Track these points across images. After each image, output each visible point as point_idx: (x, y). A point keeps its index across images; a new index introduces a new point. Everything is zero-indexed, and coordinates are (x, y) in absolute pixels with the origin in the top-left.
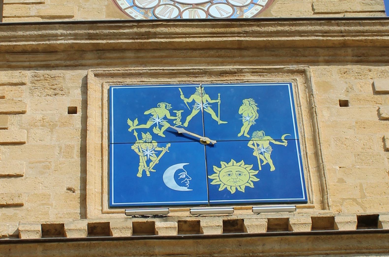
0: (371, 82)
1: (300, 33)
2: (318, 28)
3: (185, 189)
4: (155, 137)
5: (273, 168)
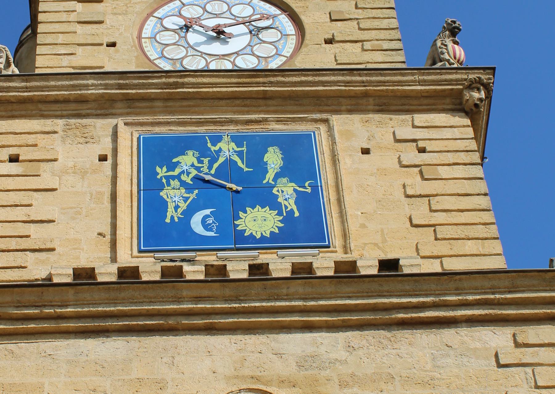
0: (392, 130)
1: (323, 83)
3: (211, 234)
4: (183, 184)
5: (297, 214)
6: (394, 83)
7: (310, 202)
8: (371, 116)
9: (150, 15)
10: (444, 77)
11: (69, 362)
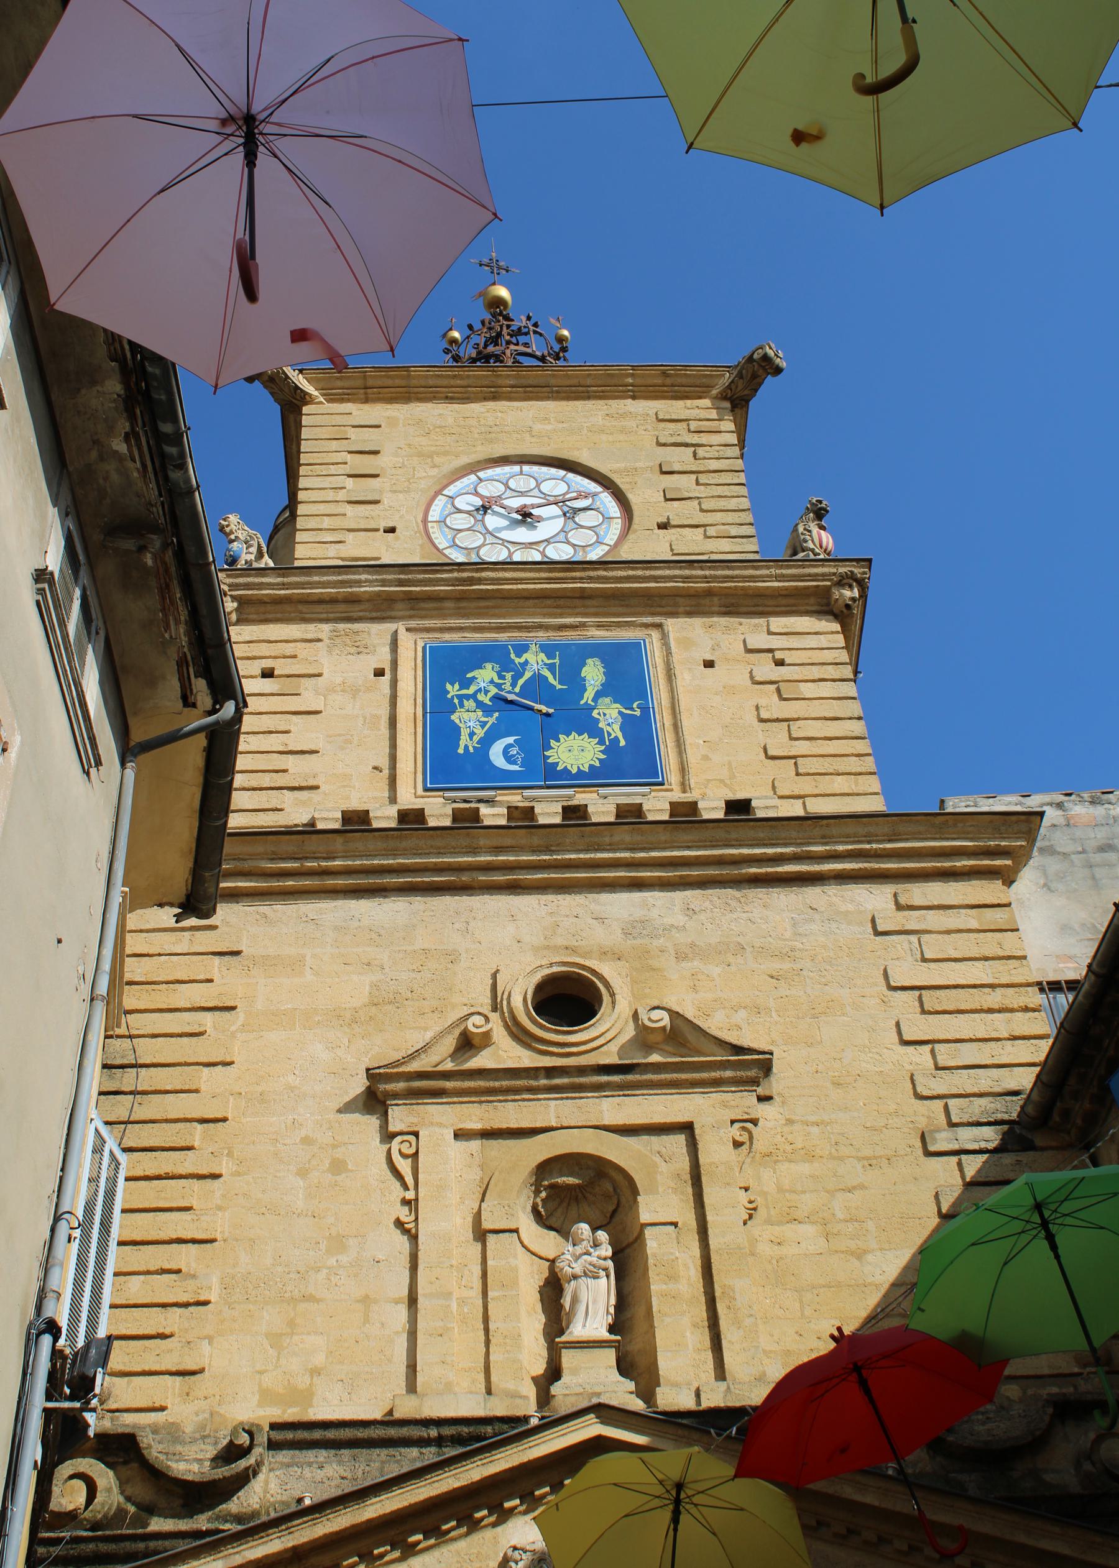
2: (677, 572)
4: (480, 705)
5: (622, 743)
6: (745, 578)
7: (640, 728)
8: (715, 619)
9: (439, 492)
11: (336, 928)
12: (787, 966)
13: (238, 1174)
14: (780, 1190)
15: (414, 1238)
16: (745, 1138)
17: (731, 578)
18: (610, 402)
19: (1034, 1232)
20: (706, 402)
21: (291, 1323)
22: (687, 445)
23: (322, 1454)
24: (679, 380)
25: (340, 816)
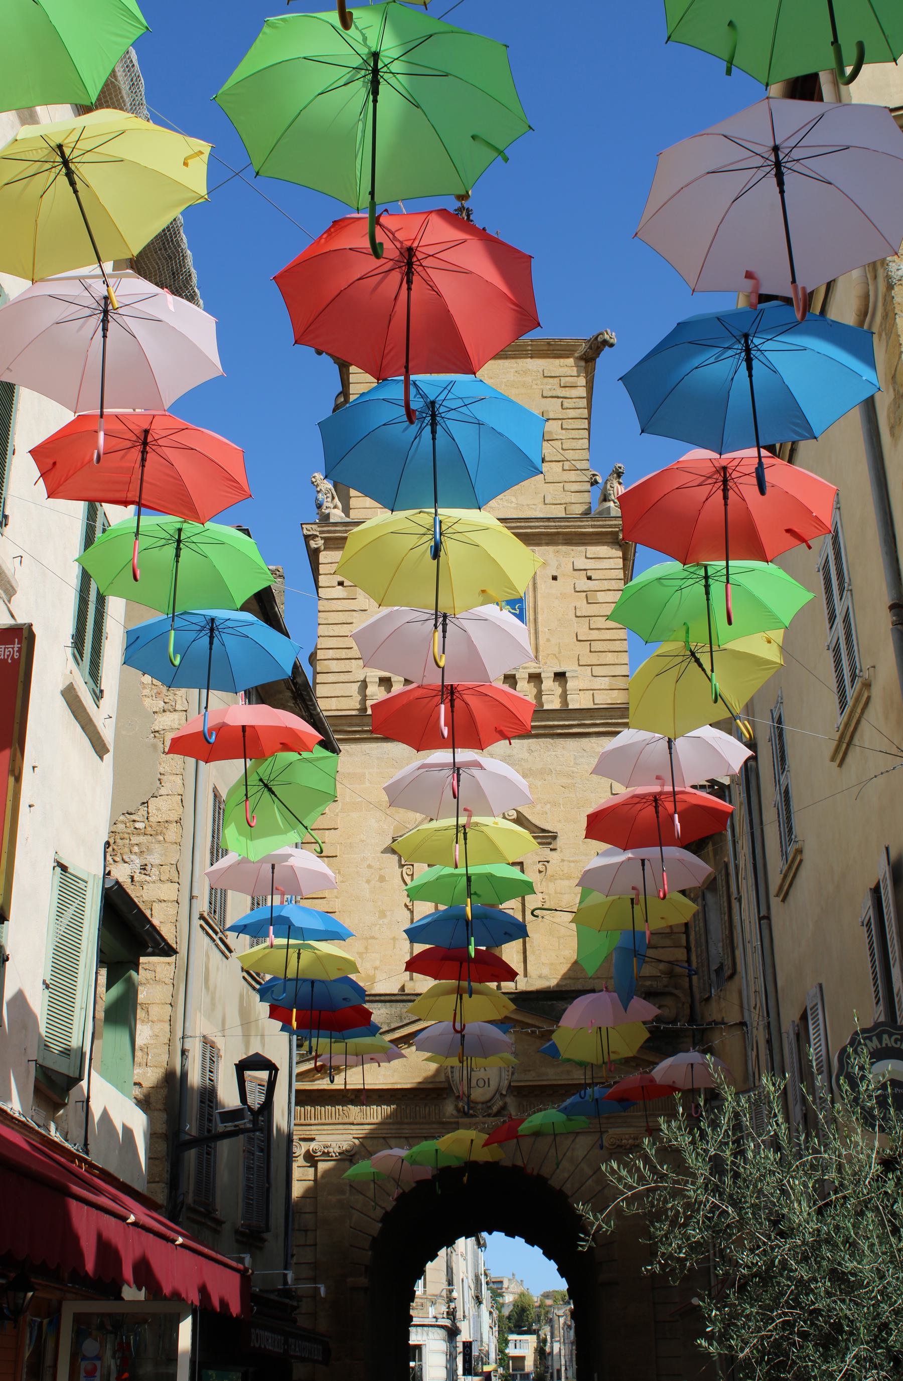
0: (572, 560)
1: (530, 527)
2: (541, 524)
6: (575, 527)
8: (560, 547)
10: (607, 523)
11: (378, 758)
12: (570, 781)
13: (342, 882)
14: (556, 893)
15: (412, 912)
16: (543, 869)
17: (568, 527)
18: (518, 360)
19: (769, 169)
20: (571, 361)
21: (366, 948)
22: (558, 397)
23: (380, 1005)
24: (557, 348)
25: (378, 680)
